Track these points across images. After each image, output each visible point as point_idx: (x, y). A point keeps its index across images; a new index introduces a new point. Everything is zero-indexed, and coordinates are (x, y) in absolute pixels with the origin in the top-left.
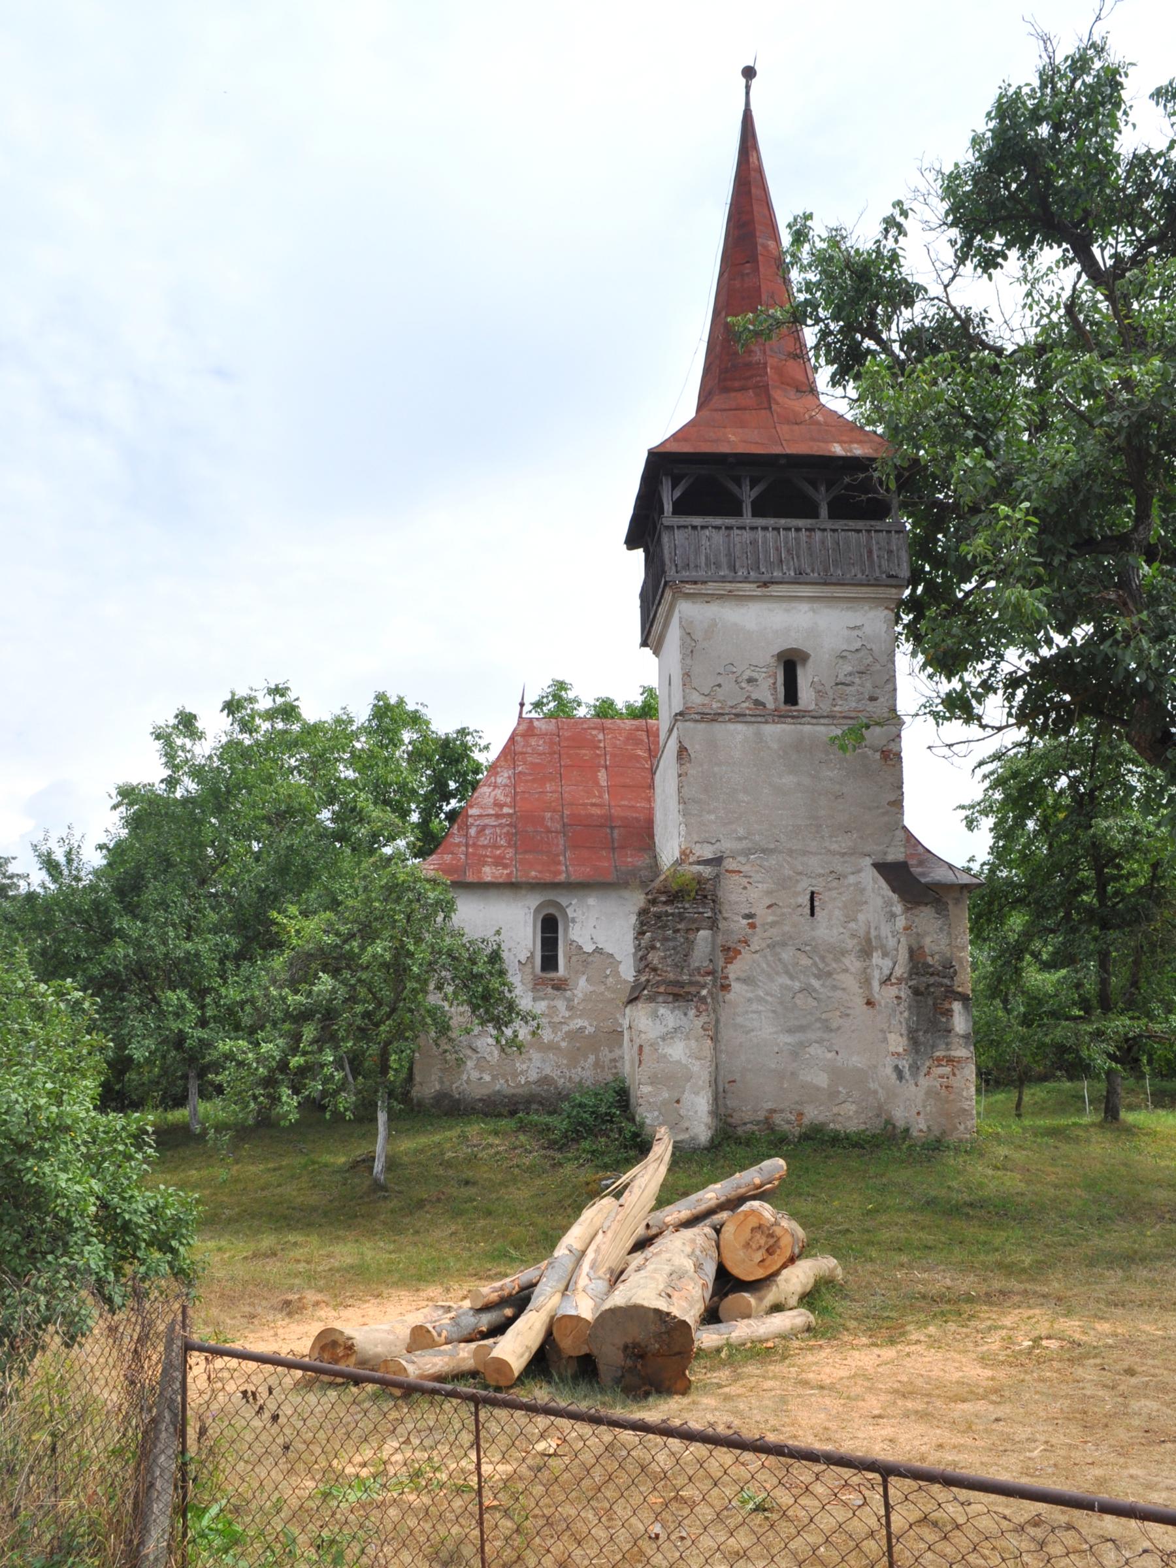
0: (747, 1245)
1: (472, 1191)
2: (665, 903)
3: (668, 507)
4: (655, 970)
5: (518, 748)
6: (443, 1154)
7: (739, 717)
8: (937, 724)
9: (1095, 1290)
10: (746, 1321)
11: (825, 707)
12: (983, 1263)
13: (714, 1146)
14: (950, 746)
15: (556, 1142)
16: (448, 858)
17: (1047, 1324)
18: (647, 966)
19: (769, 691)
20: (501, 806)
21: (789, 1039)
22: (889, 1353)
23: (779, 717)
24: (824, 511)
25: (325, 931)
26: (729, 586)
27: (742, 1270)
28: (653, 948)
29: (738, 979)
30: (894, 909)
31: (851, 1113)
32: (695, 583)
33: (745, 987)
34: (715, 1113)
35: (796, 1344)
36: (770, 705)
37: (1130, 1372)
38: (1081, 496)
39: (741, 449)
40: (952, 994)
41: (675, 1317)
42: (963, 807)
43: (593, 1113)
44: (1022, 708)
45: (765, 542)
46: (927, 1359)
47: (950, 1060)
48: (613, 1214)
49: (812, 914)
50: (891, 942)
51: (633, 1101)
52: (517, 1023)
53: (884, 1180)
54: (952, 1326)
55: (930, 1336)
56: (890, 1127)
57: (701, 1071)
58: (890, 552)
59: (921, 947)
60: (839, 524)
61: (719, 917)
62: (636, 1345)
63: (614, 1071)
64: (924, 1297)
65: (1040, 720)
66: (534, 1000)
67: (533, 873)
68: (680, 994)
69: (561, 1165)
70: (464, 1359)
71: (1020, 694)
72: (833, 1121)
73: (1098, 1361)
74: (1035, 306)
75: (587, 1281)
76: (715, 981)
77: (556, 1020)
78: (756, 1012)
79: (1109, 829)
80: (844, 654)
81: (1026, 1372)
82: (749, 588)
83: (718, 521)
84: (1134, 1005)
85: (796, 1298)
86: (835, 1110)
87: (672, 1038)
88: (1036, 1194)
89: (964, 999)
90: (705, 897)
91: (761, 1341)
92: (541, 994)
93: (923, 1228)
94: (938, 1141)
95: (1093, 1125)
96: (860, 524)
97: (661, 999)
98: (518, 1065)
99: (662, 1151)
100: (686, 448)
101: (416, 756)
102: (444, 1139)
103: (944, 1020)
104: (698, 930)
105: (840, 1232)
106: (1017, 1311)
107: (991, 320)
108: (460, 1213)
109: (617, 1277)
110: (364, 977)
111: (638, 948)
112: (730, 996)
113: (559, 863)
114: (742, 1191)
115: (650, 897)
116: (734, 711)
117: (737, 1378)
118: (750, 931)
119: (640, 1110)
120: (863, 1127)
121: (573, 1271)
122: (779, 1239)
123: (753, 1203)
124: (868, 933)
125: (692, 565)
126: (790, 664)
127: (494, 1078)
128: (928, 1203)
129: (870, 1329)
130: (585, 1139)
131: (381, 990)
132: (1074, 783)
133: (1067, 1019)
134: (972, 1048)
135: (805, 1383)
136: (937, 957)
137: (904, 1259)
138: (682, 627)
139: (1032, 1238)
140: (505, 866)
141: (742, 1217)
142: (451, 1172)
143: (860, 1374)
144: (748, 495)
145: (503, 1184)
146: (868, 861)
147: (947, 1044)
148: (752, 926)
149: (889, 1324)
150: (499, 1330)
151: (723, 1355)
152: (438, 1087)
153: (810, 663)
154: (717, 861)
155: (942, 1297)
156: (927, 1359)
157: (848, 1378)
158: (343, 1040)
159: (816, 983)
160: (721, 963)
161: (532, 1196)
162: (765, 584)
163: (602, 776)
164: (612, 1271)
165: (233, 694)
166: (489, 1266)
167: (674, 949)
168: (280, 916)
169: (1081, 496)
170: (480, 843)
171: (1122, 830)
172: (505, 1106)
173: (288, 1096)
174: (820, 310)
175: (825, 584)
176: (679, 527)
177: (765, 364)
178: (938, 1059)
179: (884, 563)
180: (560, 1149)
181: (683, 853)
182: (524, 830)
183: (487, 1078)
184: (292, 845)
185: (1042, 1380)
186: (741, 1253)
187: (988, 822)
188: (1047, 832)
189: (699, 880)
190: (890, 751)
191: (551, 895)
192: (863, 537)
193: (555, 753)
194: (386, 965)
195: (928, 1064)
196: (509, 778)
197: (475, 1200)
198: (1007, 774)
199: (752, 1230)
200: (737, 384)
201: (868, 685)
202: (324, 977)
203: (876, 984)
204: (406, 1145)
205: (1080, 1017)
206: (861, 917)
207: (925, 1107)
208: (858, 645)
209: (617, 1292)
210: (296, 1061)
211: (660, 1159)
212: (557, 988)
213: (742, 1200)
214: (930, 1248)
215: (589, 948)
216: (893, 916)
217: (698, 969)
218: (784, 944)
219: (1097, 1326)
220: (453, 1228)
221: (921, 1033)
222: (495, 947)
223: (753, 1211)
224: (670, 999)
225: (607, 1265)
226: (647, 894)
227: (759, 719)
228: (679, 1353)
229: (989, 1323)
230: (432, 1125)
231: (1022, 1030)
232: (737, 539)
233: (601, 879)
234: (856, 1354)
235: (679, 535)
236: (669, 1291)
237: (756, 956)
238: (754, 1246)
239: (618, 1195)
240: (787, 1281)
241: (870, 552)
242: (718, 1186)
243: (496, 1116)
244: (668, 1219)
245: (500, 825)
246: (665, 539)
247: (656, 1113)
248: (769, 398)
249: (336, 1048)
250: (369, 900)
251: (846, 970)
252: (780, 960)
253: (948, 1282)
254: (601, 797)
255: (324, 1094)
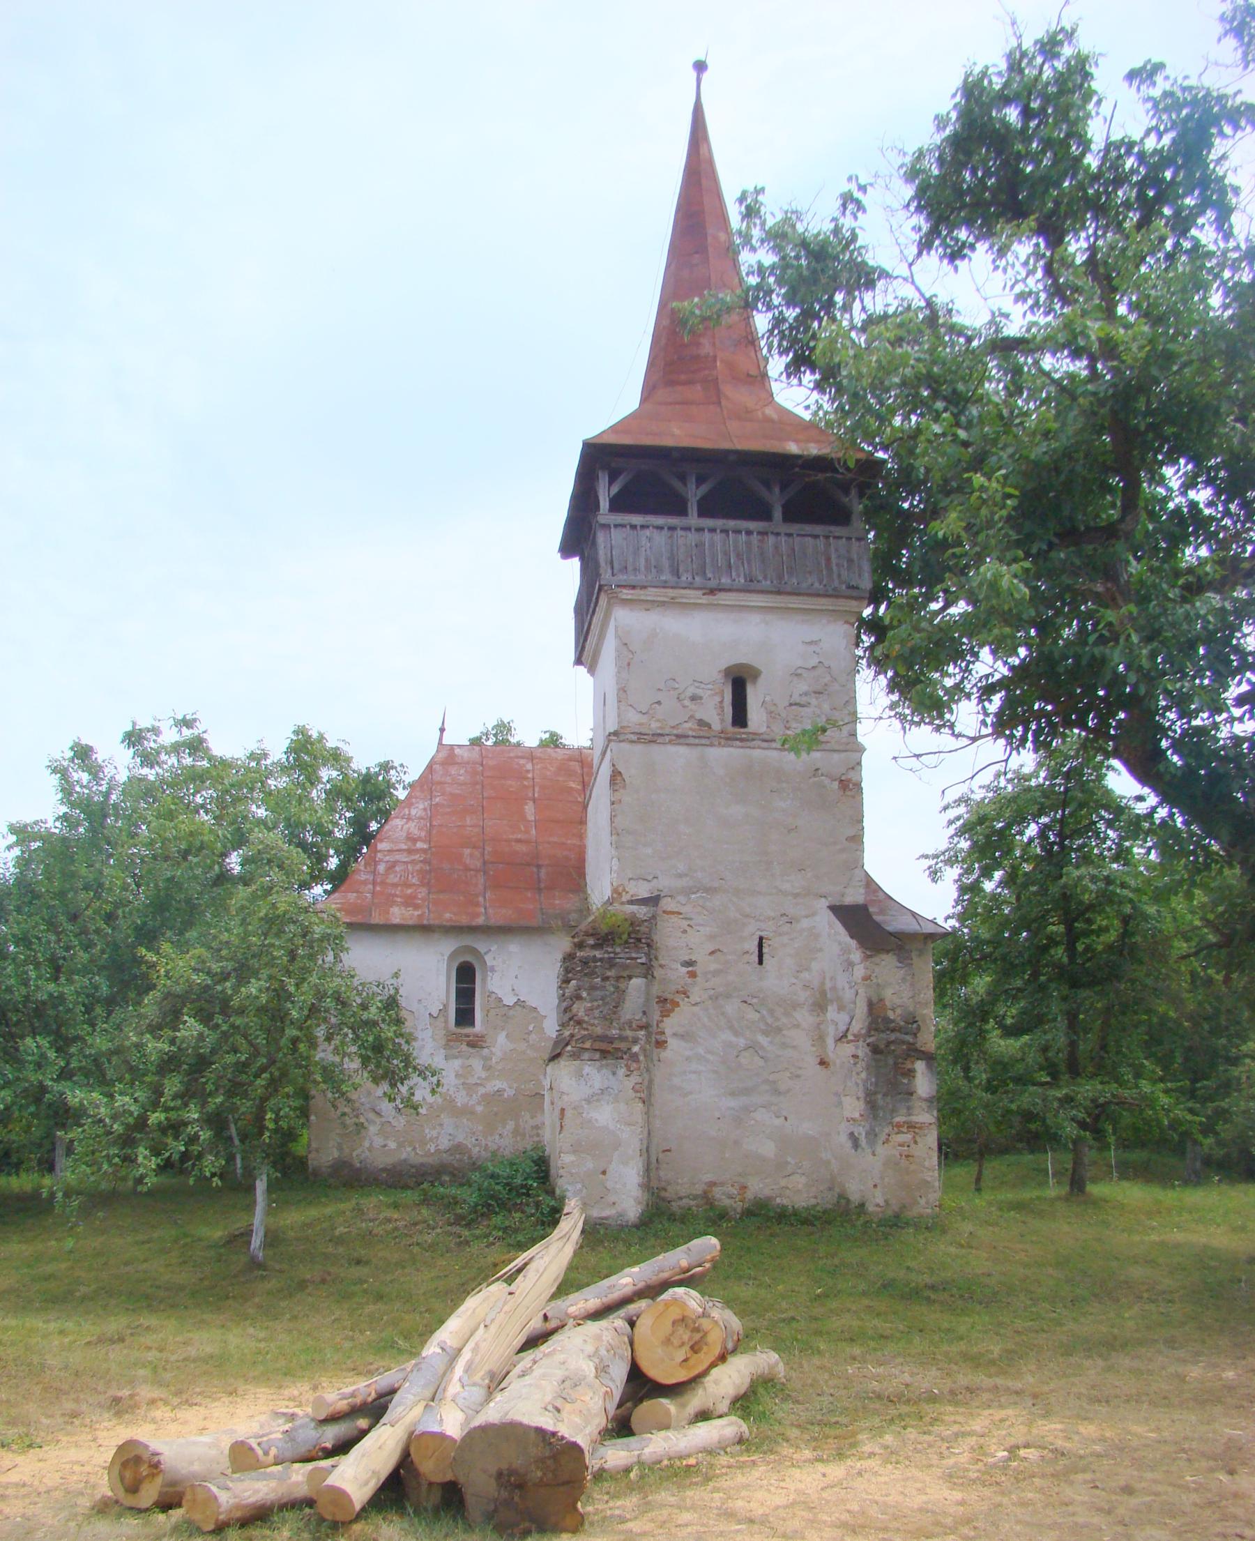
0: (667, 1341)
1: (363, 1271)
2: (593, 947)
3: (604, 504)
4: (579, 1023)
5: (437, 778)
6: (334, 1229)
7: (681, 738)
8: (904, 729)
9: (1073, 1384)
10: (663, 1433)
11: (778, 730)
12: (946, 1354)
13: (645, 1223)
14: (918, 756)
15: (462, 1217)
16: (352, 897)
17: (1023, 1429)
18: (571, 1019)
19: (716, 710)
20: (415, 840)
21: (733, 1103)
22: (836, 1471)
23: (728, 739)
24: (778, 514)
25: (194, 970)
26: (671, 593)
27: (661, 1370)
28: (579, 998)
29: (675, 1034)
30: (852, 956)
31: (800, 1186)
32: (634, 587)
33: (683, 1044)
34: (647, 1186)
35: (724, 1460)
36: (717, 726)
37: (1128, 1490)
38: (1063, 477)
39: (686, 443)
40: (915, 1052)
41: (563, 1438)
42: (926, 857)
43: (508, 1184)
44: (999, 714)
45: (712, 545)
46: (882, 1479)
47: (911, 1126)
48: (500, 1304)
49: (761, 962)
50: (848, 995)
51: (553, 1171)
52: (415, 1079)
53: (836, 1261)
54: (911, 1433)
55: (886, 1447)
56: (843, 1202)
57: (632, 1139)
58: (850, 561)
59: (881, 1000)
60: (794, 528)
61: (654, 963)
62: (512, 1472)
63: (536, 1139)
64: (879, 1397)
65: (1018, 732)
66: (447, 1058)
67: (448, 915)
68: (608, 1050)
69: (467, 1243)
70: (297, 1484)
71: (997, 699)
72: (780, 1196)
73: (1088, 1476)
74: (1009, 269)
75: (458, 1387)
76: (649, 1035)
77: (471, 1081)
78: (695, 1071)
79: (1080, 878)
80: (799, 671)
81: (1003, 1493)
82: (694, 596)
83: (660, 520)
84: (1104, 1069)
85: (727, 1402)
86: (783, 1183)
87: (598, 1100)
88: (1004, 1274)
89: (929, 1058)
90: (639, 940)
91: (680, 1458)
92: (455, 1052)
93: (878, 1315)
94: (897, 1216)
95: (1059, 1198)
96: (818, 529)
97: (586, 1056)
98: (427, 1131)
99: (570, 1227)
100: (626, 440)
101: (336, 793)
102: (333, 1212)
103: (905, 1081)
104: (630, 978)
105: (784, 1320)
106: (986, 1412)
107: (958, 311)
108: (348, 1296)
109: (496, 1382)
110: (238, 1022)
111: (562, 997)
112: (666, 1054)
113: (478, 905)
114: (665, 1275)
115: (576, 940)
116: (675, 732)
117: (646, 1507)
118: (690, 980)
119: (560, 1182)
120: (813, 1201)
121: (444, 1374)
122: (706, 1334)
123: (677, 1290)
124: (823, 984)
125: (630, 568)
126: (740, 683)
127: (401, 1145)
128: (884, 1286)
129: (815, 1439)
130: (497, 1213)
131: (257, 1037)
132: (1042, 834)
133: (1034, 1084)
134: (935, 1113)
135: (730, 1515)
136: (899, 1011)
137: (857, 1351)
138: (617, 637)
139: (1000, 1324)
140: (416, 907)
141: (661, 1307)
142: (341, 1249)
143: (802, 1502)
144: (694, 493)
145: (401, 1264)
146: (824, 903)
147: (909, 1108)
148: (693, 975)
149: (838, 1432)
150: (343, 1447)
151: (632, 1475)
152: (336, 1154)
153: (761, 681)
154: (653, 901)
155: (900, 1396)
156: (882, 1479)
157: (786, 1507)
158: (210, 1094)
159: (762, 1040)
160: (656, 1017)
161: (432, 1279)
162: (712, 592)
163: (529, 809)
164: (492, 1375)
165: (134, 724)
166: (370, 1358)
167: (602, 999)
168: (149, 954)
169: (1063, 477)
170: (389, 881)
171: (1094, 879)
172: (411, 1177)
173: (145, 1157)
174: (774, 296)
175: (779, 593)
176: (616, 526)
177: (715, 357)
178: (899, 1125)
179: (844, 573)
180: (468, 1225)
181: (615, 891)
182: (440, 868)
183: (392, 1145)
184: (173, 877)
185: (1024, 1504)
186: (659, 1350)
187: (952, 873)
188: (1015, 883)
189: (633, 922)
190: (849, 781)
191: (467, 941)
192: (821, 543)
193: (476, 783)
194: (262, 1010)
195: (886, 1130)
196: (425, 809)
197: (366, 1281)
198: (974, 819)
199: (674, 1323)
200: (683, 377)
201: (826, 707)
202: (191, 1021)
203: (830, 1042)
204: (293, 1218)
205: (1047, 1083)
206: (815, 966)
207: (882, 1178)
208: (813, 662)
209: (492, 1404)
210: (156, 1117)
211: (567, 1236)
212: (472, 1045)
213: (665, 1285)
214: (886, 1337)
215: (510, 1000)
216: (851, 964)
217: (630, 1023)
218: (728, 996)
219: (1082, 1429)
220: (338, 1313)
221: (879, 1096)
222: (392, 992)
223: (675, 1300)
224: (597, 1056)
225: (486, 1368)
226: (573, 937)
227: (703, 741)
228: (568, 1482)
229: (956, 1428)
230: (327, 1196)
231: (987, 1096)
232: (681, 541)
233: (523, 923)
234: (796, 1472)
235: (617, 536)
236: (559, 1403)
237: (696, 1009)
238: (676, 1342)
239: (510, 1279)
240: (716, 1382)
241: (828, 560)
242: (636, 1269)
243: (402, 1188)
244: (572, 1310)
245: (412, 862)
246: (601, 538)
247: (579, 1186)
248: (718, 393)
249: (204, 1104)
250: (247, 934)
251: (797, 1026)
252: (723, 1014)
253: (907, 1378)
254: (527, 832)
255: (185, 1156)
